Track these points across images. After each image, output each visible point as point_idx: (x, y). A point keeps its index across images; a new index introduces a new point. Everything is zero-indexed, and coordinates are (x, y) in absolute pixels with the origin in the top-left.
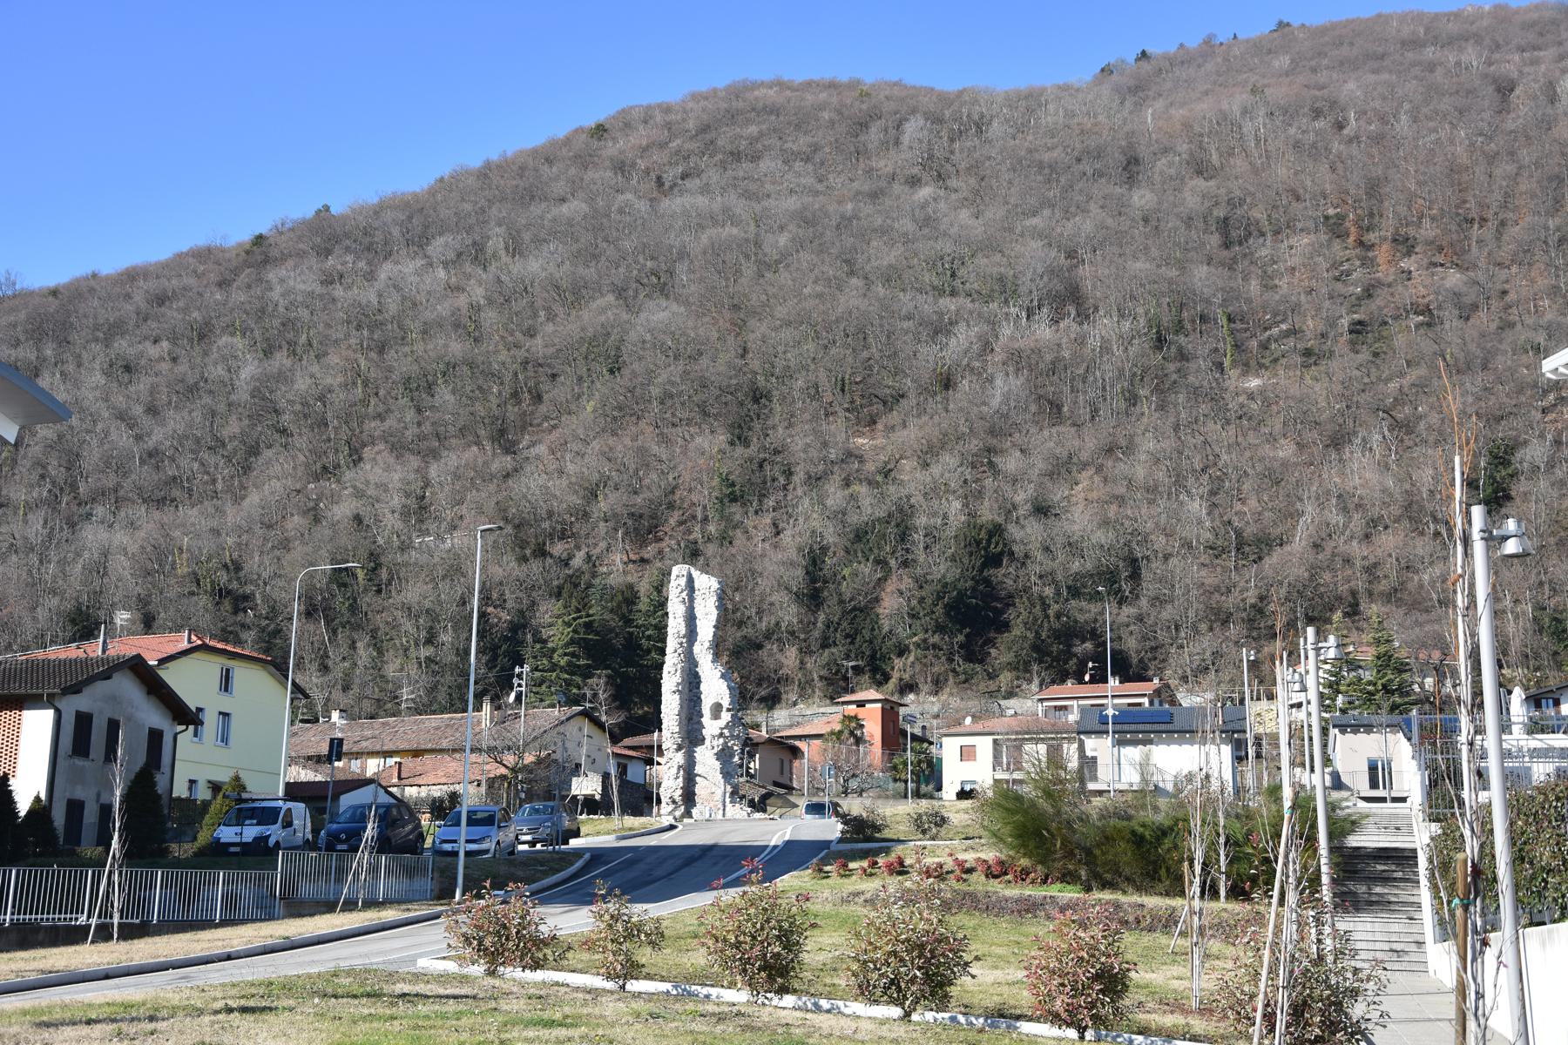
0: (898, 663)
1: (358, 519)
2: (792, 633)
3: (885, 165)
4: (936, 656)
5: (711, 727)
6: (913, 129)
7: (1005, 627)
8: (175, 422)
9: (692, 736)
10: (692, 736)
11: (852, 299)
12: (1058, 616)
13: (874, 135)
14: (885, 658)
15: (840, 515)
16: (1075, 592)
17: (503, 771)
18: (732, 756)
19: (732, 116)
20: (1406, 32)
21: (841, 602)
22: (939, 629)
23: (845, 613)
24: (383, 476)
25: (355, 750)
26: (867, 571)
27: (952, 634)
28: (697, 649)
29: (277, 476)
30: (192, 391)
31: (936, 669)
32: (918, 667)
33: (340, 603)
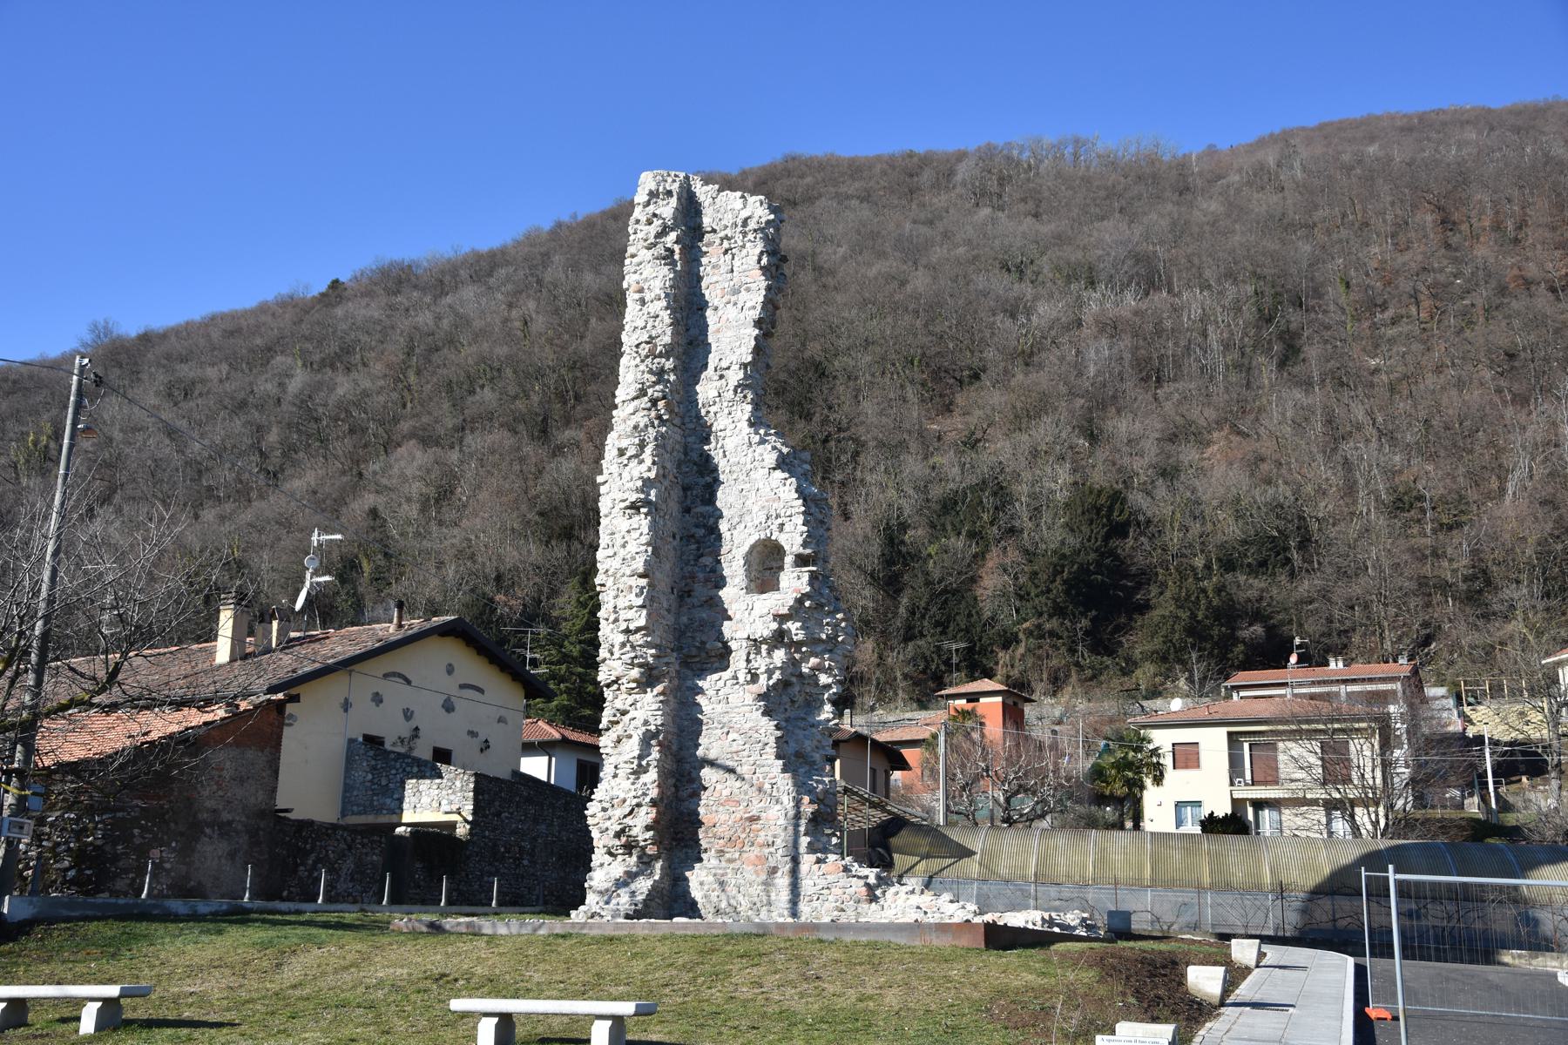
1: (374, 513)
2: (867, 623)
4: (1054, 646)
5: (748, 614)
6: (963, 172)
7: (1145, 607)
9: (688, 642)
11: (920, 281)
12: (1220, 589)
13: (926, 176)
16: (1229, 565)
18: (814, 704)
19: (788, 173)
22: (1058, 611)
24: (410, 462)
26: (960, 544)
28: (706, 390)
31: (1054, 662)
32: (1030, 661)
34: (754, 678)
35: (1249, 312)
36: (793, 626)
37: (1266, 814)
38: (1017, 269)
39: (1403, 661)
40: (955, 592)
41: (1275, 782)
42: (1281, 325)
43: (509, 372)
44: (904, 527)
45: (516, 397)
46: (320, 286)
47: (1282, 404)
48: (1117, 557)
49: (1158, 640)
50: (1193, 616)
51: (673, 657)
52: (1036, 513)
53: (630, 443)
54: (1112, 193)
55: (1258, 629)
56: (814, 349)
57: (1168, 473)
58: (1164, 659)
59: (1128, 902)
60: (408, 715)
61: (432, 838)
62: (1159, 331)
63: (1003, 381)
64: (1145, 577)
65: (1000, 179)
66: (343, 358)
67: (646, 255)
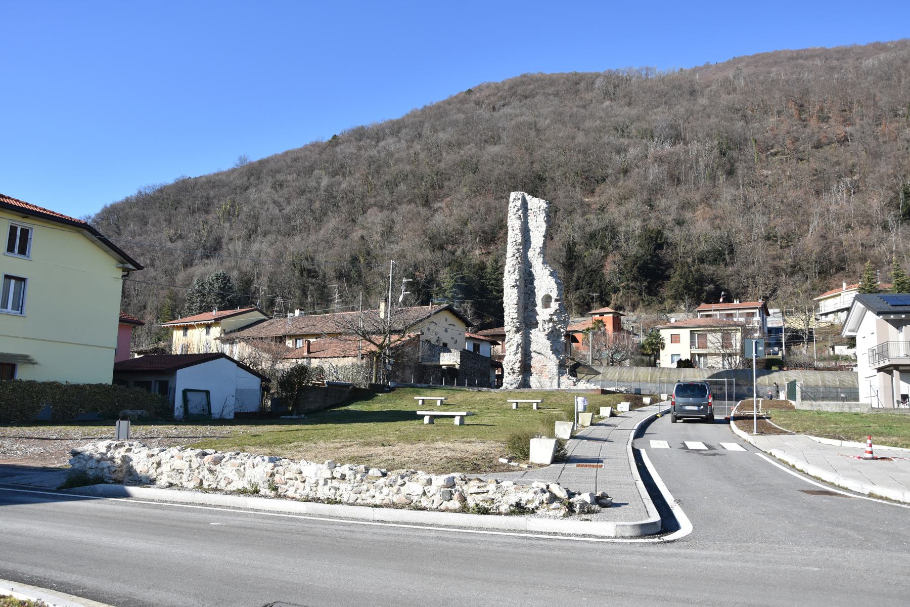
0: (614, 296)
1: (362, 237)
3: (588, 96)
5: (543, 314)
6: (598, 83)
7: (668, 278)
8: (295, 203)
9: (528, 321)
10: (528, 321)
11: (581, 138)
12: (697, 271)
13: (582, 85)
14: (607, 294)
15: (582, 228)
16: (702, 261)
17: (374, 348)
18: (559, 336)
19: (523, 83)
20: (788, 55)
21: (585, 267)
22: (635, 279)
23: (586, 273)
24: (375, 218)
25: (298, 333)
27: (641, 282)
28: (530, 254)
29: (332, 222)
30: (303, 192)
31: (633, 299)
32: (624, 298)
33: (353, 274)
34: (544, 330)
35: (716, 152)
36: (554, 317)
37: (702, 359)
38: (621, 130)
39: (760, 301)
40: (595, 271)
41: (706, 347)
42: (728, 159)
43: (411, 176)
44: (575, 244)
45: (414, 188)
46: (328, 138)
47: (727, 192)
48: (659, 257)
49: (673, 291)
50: (687, 282)
51: (523, 325)
52: (627, 240)
53: (512, 270)
54: (662, 94)
55: (712, 286)
56: (537, 167)
57: (680, 223)
58: (675, 298)
59: (642, 386)
60: (436, 334)
61: (451, 369)
62: (678, 161)
63: (615, 183)
64: (669, 265)
65: (616, 87)
66: (340, 170)
67: (514, 217)
